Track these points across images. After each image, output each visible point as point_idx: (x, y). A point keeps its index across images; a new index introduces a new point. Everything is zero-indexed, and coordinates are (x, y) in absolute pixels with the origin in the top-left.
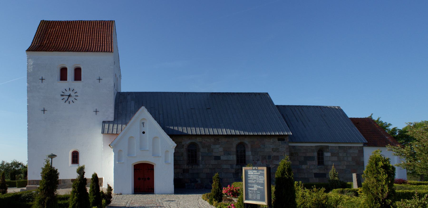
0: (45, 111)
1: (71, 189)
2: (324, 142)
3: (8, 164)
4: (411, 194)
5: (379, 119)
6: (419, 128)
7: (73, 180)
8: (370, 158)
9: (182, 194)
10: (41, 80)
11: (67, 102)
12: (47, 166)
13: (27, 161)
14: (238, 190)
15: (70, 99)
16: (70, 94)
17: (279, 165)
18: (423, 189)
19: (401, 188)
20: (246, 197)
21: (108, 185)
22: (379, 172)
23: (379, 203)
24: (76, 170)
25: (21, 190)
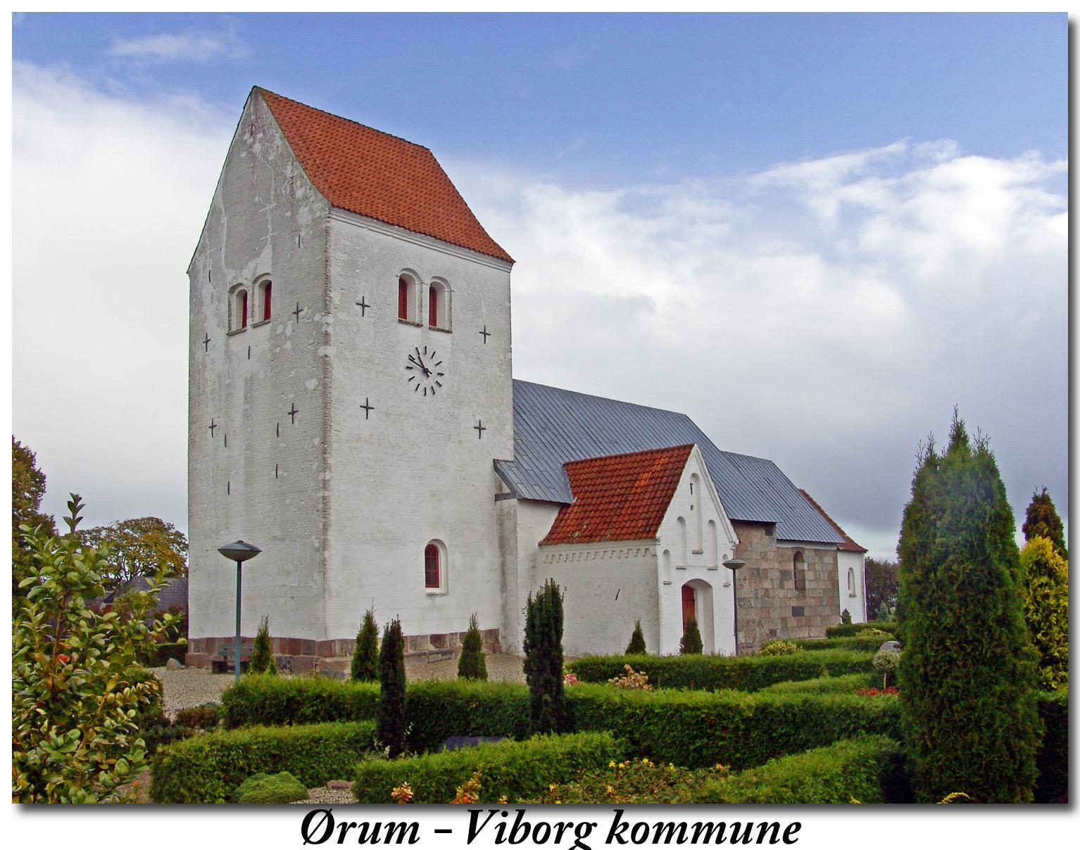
0: (291, 411)
1: (755, 540)
2: (739, 627)
3: (1013, 536)
4: (920, 506)
5: (474, 622)
6: (57, 704)
7: (462, 634)
8: (369, 628)
9: (404, 677)
10: (487, 332)
11: (411, 359)
12: (547, 587)
13: (959, 437)
14: (973, 556)
15: (417, 373)
16: (475, 428)
17: (105, 780)
18: (733, 782)
19: (257, 315)
20: (507, 304)
21: (369, 619)
22: (553, 603)
23: (146, 744)
24: (49, 515)
25: (176, 641)
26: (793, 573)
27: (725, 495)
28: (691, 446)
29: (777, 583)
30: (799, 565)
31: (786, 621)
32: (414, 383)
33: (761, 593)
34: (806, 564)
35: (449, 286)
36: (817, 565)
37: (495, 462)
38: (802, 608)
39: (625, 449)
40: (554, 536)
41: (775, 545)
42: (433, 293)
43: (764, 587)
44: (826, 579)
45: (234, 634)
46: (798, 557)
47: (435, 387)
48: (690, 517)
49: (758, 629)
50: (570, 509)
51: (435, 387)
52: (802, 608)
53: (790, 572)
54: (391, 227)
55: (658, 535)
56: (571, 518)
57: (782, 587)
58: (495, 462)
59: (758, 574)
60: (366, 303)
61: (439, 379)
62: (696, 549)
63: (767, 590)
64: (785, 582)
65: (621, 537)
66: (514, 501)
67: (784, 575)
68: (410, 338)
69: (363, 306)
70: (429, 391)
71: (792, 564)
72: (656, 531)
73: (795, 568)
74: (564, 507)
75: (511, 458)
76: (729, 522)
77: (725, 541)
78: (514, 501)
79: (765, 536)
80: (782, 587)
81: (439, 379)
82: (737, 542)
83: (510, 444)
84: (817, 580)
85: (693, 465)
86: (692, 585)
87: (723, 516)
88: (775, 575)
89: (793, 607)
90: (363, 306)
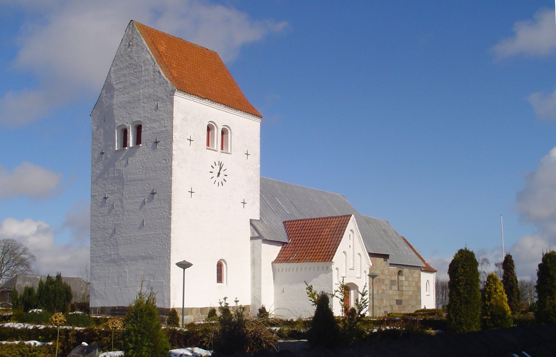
26: (397, 282)
27: (367, 239)
28: (351, 216)
29: (388, 286)
30: (400, 277)
31: (393, 307)
32: (214, 179)
33: (380, 291)
34: (404, 277)
35: (231, 130)
36: (409, 278)
37: (251, 220)
38: (401, 301)
39: (287, 218)
40: (280, 259)
41: (388, 266)
42: (223, 133)
43: (382, 288)
44: (414, 285)
45: (182, 307)
46: (400, 273)
47: (223, 182)
48: (350, 252)
49: (378, 311)
50: (288, 245)
51: (223, 182)
52: (401, 301)
53: (396, 281)
54: (204, 100)
55: (333, 260)
56: (288, 250)
57: (391, 289)
58: (251, 220)
59: (379, 281)
60: (191, 139)
61: (225, 178)
62: (352, 267)
63: (383, 290)
64: (393, 286)
65: (281, 261)
66: (260, 241)
67: (392, 282)
68: (216, 156)
69: (190, 140)
70: (220, 184)
71: (397, 277)
72: (332, 258)
73: (398, 279)
74: (283, 244)
75: (259, 219)
76: (368, 254)
77: (366, 263)
78: (260, 241)
79: (383, 262)
80: (391, 289)
81: (225, 178)
82: (371, 264)
83: (258, 212)
84: (410, 286)
85: (352, 224)
86: (349, 286)
87: (365, 251)
88: (387, 282)
89: (397, 300)
90: (190, 140)
